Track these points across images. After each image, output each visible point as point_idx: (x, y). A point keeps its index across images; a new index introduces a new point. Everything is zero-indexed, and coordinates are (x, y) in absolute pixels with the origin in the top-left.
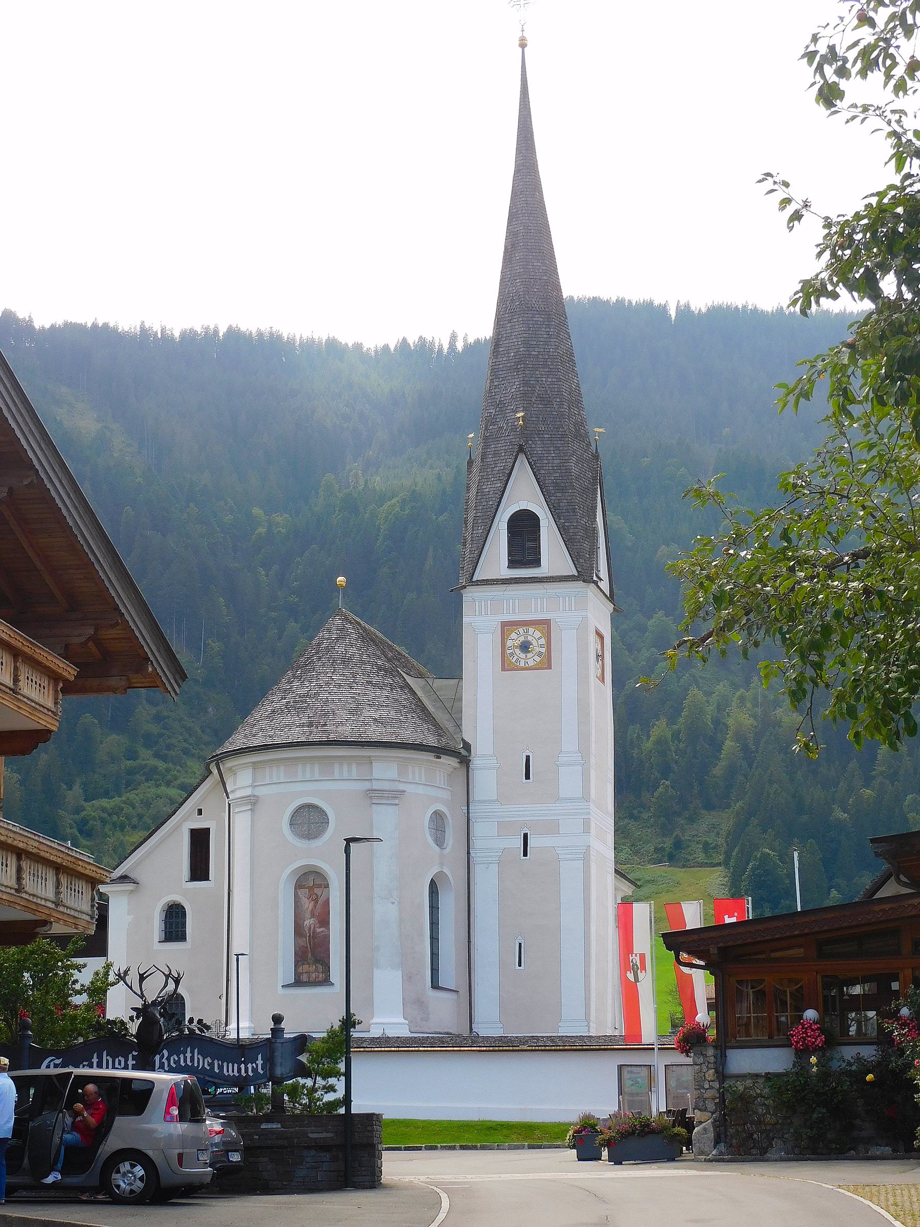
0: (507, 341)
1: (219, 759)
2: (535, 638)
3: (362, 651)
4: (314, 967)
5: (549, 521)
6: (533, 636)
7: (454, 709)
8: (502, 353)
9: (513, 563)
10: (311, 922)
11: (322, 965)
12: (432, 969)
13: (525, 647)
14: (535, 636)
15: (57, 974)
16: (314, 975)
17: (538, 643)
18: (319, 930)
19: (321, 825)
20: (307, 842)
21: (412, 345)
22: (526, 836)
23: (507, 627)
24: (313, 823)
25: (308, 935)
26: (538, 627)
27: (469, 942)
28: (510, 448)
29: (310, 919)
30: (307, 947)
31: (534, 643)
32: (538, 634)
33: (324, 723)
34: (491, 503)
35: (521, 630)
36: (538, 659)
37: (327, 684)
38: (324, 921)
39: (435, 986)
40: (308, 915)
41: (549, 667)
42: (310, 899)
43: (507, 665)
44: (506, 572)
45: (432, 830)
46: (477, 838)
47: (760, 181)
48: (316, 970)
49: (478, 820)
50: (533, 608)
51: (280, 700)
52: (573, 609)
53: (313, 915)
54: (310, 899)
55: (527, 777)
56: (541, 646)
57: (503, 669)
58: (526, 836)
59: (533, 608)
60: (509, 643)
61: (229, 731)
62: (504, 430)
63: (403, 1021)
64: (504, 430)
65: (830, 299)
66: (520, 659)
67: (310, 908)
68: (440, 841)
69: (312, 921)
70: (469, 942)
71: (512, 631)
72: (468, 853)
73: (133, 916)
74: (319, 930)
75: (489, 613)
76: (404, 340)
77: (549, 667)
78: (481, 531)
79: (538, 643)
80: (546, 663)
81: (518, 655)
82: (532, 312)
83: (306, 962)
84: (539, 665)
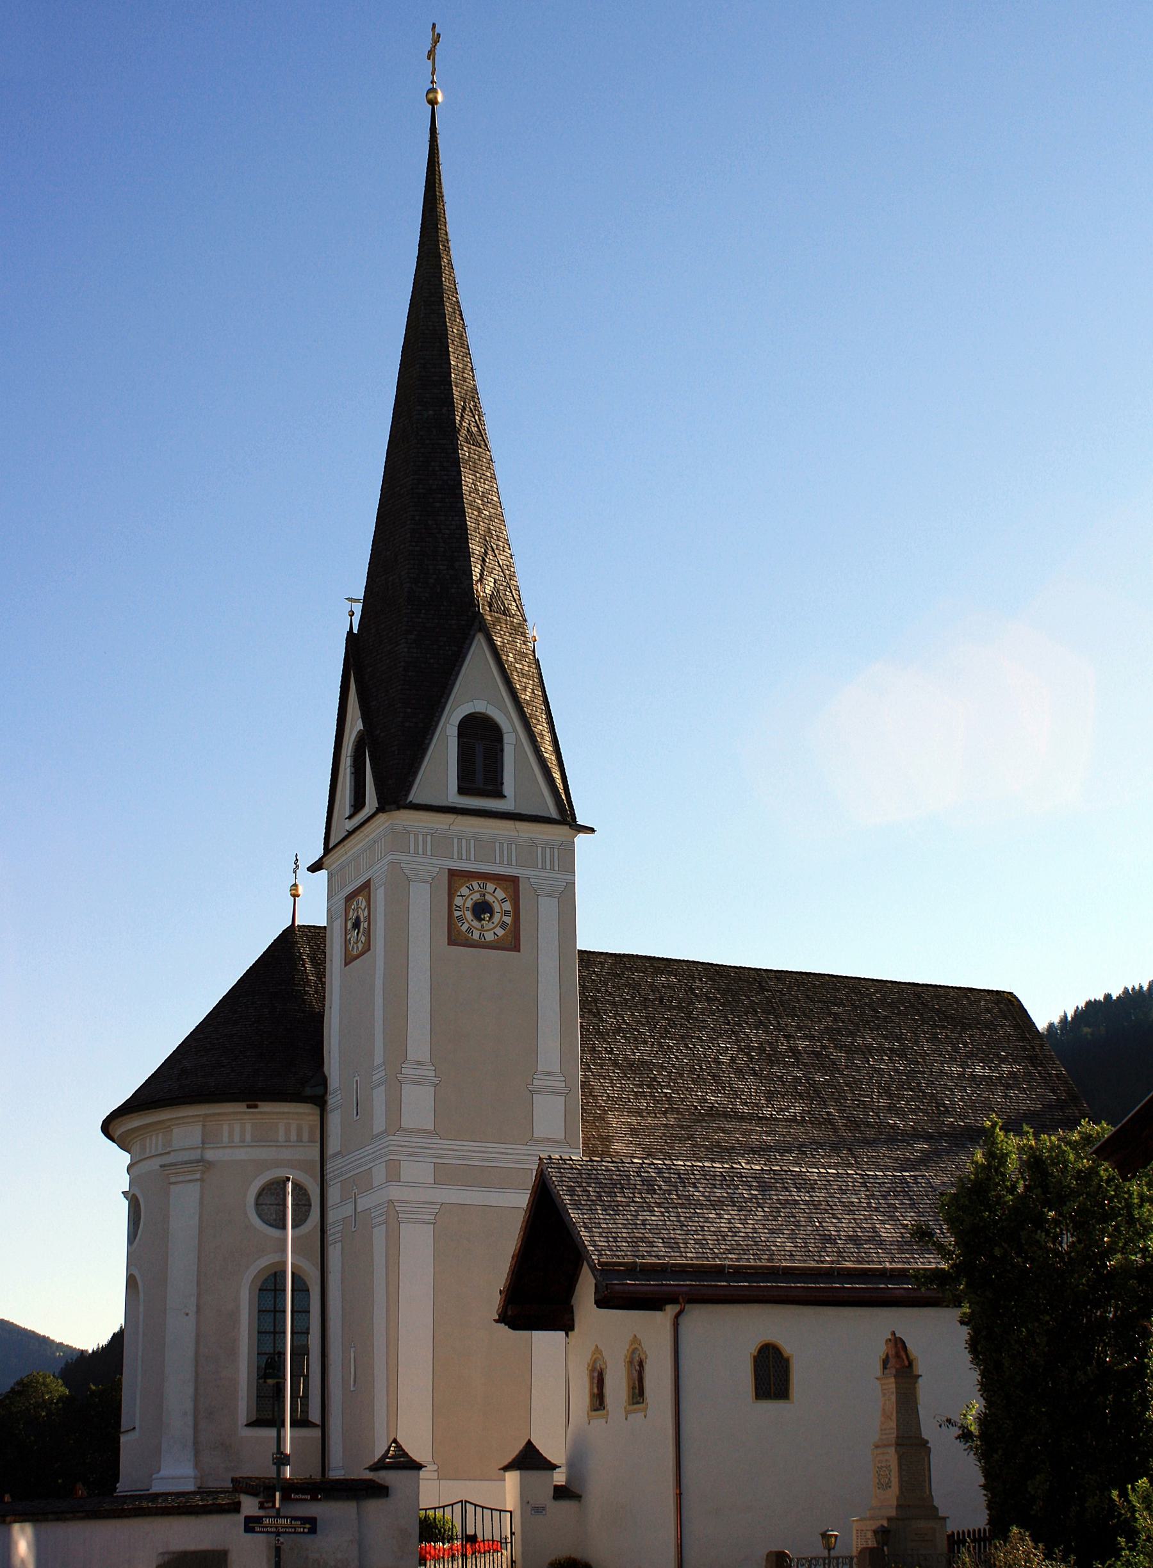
2: (498, 900)
13: (482, 909)
14: (496, 896)
15: (1091, 1205)
17: (501, 906)
32: (500, 894)
35: (475, 884)
36: (500, 932)
41: (516, 948)
43: (455, 938)
44: (453, 797)
47: (434, 25)
52: (556, 868)
56: (507, 913)
57: (452, 942)
60: (458, 901)
66: (473, 929)
75: (556, 868)
77: (516, 948)
79: (501, 906)
80: (512, 942)
81: (494, 925)
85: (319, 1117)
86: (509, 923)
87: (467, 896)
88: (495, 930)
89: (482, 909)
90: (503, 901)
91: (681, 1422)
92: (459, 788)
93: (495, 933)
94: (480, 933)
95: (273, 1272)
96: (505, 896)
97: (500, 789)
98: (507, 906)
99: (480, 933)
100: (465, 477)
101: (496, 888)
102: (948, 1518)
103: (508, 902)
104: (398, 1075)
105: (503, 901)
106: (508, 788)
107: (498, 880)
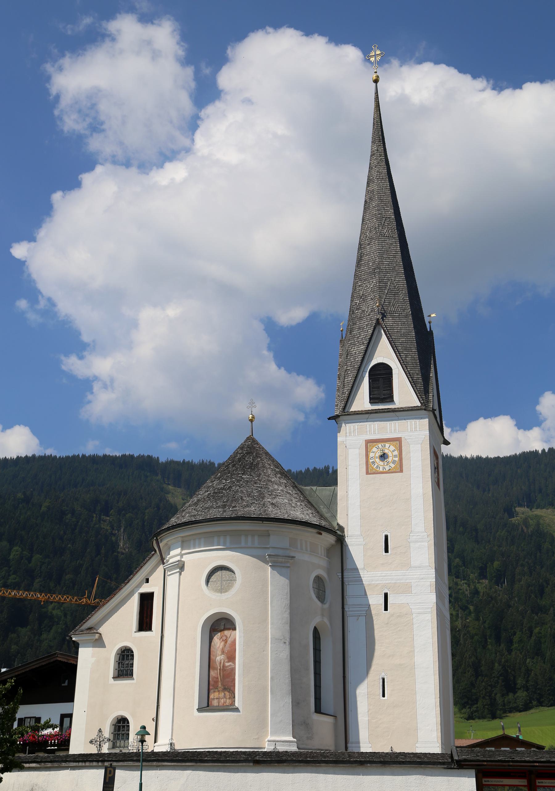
0: (367, 257)
1: (159, 533)
3: (265, 461)
4: (223, 694)
5: (399, 370)
6: (389, 450)
7: (333, 501)
8: (363, 264)
9: (373, 400)
10: (222, 658)
11: (229, 692)
12: (316, 698)
13: (383, 457)
14: (390, 449)
16: (222, 701)
18: (227, 664)
19: (231, 582)
20: (220, 594)
21: (311, 471)
22: (386, 595)
23: (369, 443)
24: (224, 581)
25: (219, 668)
26: (392, 443)
27: (344, 677)
28: (371, 322)
29: (221, 655)
30: (217, 678)
31: (390, 454)
32: (392, 448)
33: (234, 506)
34: (357, 360)
35: (380, 446)
37: (238, 481)
38: (231, 658)
39: (318, 710)
40: (219, 652)
41: (401, 471)
42: (221, 640)
44: (368, 406)
45: (316, 590)
46: (350, 597)
48: (225, 697)
49: (350, 583)
50: (388, 430)
51: (204, 493)
53: (223, 652)
54: (221, 640)
55: (386, 551)
56: (395, 456)
57: (367, 473)
58: (386, 595)
59: (388, 430)
60: (371, 455)
61: (168, 519)
62: (365, 312)
63: (291, 739)
64: (365, 312)
65: (484, 457)
66: (379, 466)
67: (221, 647)
68: (321, 597)
69: (222, 657)
70: (344, 677)
71: (373, 446)
72: (343, 608)
73: (96, 658)
74: (227, 664)
76: (308, 468)
77: (401, 471)
78: (350, 379)
82: (385, 238)
83: (217, 690)
84: (393, 470)
85: (344, 576)
86: (397, 460)
87: (375, 452)
88: (390, 465)
89: (383, 457)
90: (393, 451)
91: (347, 676)
92: (370, 399)
93: (390, 466)
94: (383, 467)
95: (312, 588)
96: (395, 449)
97: (450, 554)
98: (396, 453)
99: (383, 467)
100: (386, 177)
101: (390, 446)
102: (135, 632)
103: (396, 451)
104: (408, 540)
105: (393, 451)
106: (396, 398)
107: (400, 460)
